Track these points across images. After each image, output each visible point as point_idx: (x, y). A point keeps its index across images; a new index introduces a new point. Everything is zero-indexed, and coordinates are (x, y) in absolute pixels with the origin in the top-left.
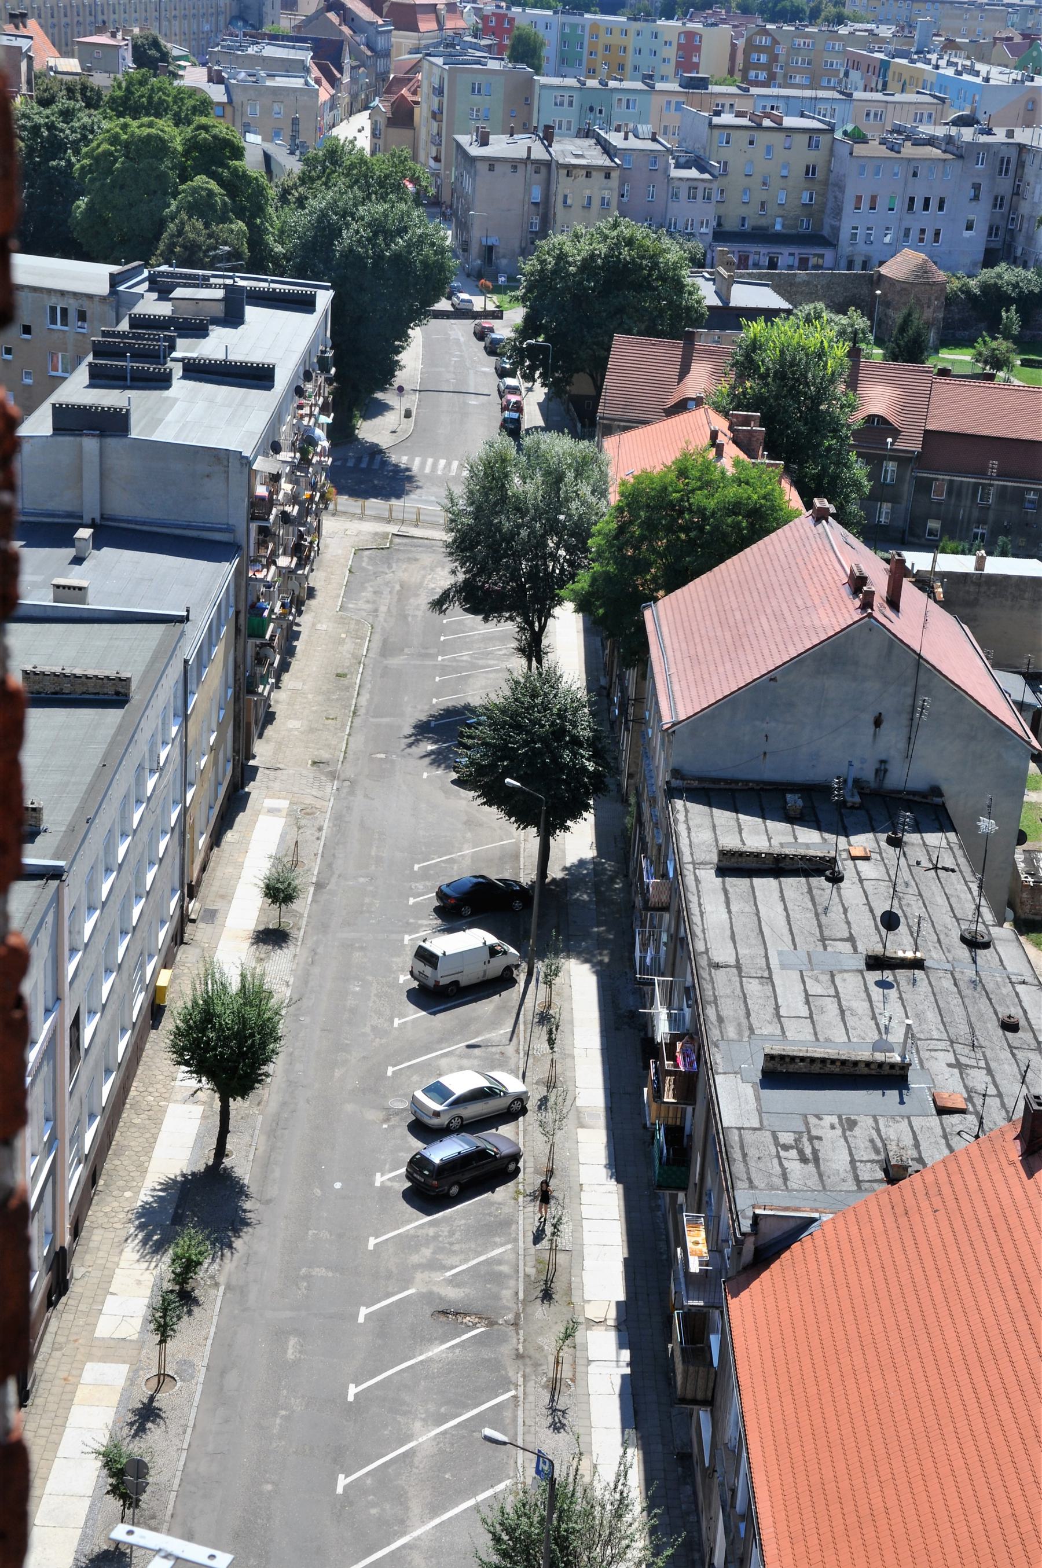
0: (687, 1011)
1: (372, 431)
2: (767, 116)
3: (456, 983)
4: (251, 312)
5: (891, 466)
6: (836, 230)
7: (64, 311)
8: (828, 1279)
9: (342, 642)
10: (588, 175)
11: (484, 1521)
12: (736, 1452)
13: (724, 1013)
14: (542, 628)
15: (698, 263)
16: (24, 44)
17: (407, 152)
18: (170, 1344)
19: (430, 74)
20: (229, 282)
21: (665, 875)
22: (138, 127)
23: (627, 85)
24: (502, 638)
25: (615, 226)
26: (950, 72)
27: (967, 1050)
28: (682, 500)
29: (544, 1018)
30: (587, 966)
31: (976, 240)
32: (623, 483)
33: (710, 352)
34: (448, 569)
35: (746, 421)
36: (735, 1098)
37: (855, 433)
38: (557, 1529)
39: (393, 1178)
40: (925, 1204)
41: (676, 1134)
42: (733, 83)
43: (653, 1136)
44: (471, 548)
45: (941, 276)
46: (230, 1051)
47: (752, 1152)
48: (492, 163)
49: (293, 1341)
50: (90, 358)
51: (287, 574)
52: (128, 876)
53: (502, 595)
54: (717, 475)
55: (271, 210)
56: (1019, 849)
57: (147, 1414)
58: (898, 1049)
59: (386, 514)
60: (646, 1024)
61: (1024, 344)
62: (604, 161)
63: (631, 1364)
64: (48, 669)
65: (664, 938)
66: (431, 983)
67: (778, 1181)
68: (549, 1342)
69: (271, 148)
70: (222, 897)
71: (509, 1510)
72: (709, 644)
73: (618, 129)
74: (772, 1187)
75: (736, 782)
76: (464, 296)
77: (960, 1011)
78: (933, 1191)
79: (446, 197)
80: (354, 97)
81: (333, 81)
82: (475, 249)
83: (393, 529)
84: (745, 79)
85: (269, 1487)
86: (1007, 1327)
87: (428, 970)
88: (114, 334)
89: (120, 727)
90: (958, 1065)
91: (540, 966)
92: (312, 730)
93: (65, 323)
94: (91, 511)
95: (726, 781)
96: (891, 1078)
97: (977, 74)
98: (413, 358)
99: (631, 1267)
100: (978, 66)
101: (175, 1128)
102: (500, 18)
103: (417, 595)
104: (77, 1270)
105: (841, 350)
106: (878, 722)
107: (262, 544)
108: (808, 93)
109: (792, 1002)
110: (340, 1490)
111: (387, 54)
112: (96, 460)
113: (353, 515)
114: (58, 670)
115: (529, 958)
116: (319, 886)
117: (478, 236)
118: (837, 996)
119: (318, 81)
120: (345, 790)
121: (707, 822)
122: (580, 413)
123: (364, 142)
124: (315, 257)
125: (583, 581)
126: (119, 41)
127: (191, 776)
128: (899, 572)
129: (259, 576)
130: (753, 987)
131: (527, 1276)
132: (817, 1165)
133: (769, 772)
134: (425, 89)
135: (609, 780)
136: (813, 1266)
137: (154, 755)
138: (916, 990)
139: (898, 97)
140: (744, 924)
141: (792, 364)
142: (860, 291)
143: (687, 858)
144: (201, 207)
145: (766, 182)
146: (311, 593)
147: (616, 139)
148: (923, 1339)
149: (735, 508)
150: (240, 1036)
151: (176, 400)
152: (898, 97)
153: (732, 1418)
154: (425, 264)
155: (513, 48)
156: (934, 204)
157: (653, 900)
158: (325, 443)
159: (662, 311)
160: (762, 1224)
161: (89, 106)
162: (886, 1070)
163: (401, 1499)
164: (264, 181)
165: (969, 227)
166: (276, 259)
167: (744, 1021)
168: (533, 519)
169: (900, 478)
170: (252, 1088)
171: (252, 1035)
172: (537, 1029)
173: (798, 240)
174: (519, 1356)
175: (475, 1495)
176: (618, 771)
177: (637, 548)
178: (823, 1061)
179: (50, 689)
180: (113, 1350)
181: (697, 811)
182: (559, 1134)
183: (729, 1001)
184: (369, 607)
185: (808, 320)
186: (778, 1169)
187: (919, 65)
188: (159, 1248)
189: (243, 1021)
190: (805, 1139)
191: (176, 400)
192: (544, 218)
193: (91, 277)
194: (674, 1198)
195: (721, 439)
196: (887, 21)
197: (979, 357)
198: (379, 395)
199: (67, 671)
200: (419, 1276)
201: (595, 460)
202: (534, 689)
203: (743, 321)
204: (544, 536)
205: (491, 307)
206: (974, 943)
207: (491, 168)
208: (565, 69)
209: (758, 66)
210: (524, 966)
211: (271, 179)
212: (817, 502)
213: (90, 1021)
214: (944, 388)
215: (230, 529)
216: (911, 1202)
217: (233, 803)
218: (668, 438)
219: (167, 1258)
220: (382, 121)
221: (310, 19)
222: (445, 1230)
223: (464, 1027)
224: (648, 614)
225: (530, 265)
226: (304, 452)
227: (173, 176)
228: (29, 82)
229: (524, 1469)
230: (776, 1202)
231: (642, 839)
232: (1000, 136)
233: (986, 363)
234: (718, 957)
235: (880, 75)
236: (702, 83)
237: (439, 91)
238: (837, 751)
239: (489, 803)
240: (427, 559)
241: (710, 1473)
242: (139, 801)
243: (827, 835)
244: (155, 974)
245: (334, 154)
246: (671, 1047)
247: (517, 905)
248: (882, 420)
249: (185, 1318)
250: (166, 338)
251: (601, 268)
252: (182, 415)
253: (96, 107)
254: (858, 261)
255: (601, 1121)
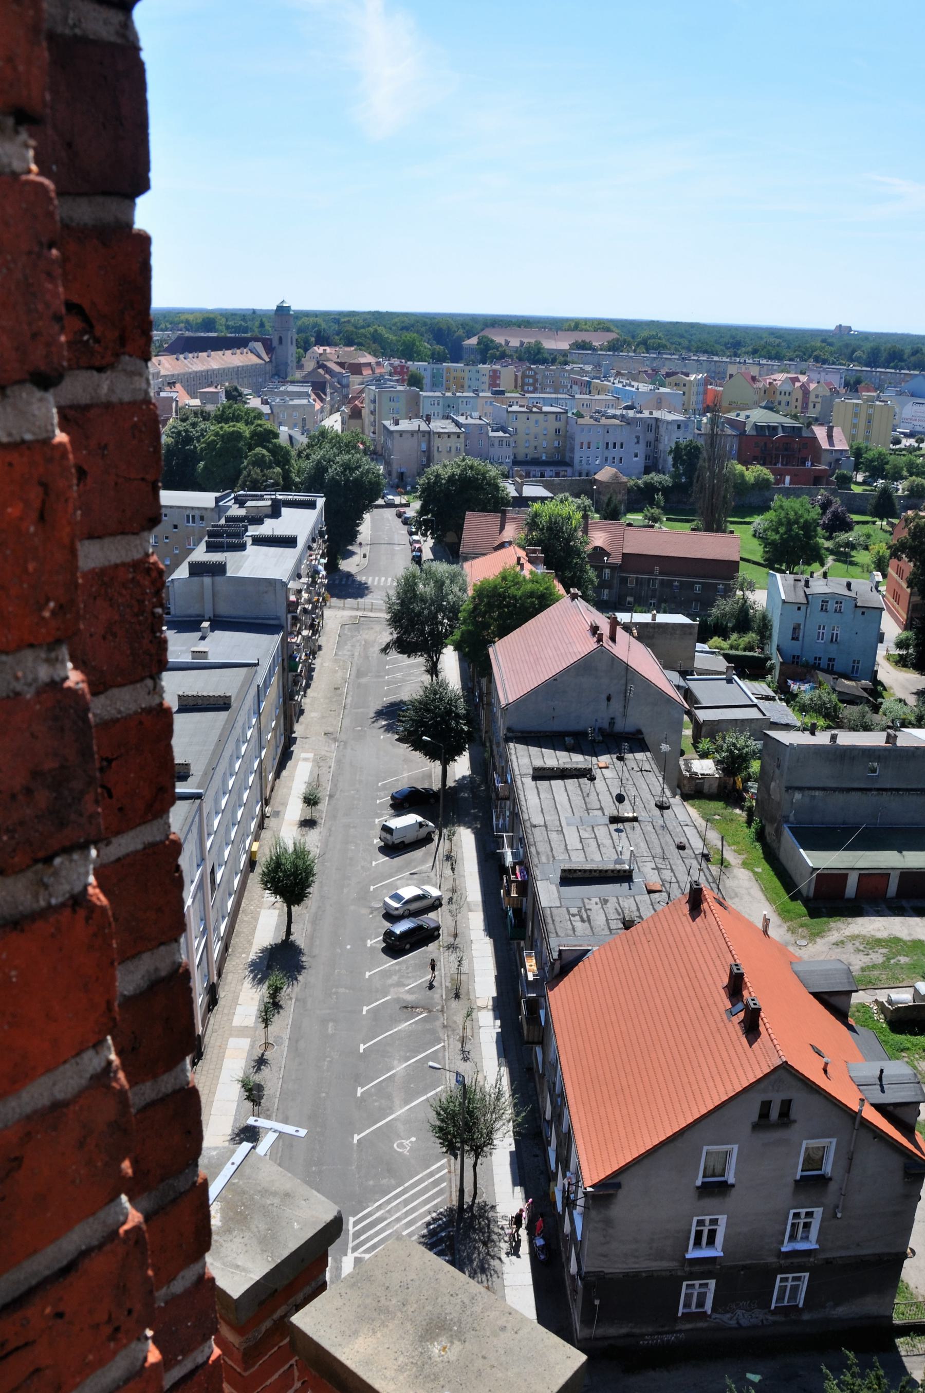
0: (521, 850)
1: (346, 565)
2: (535, 406)
3: (403, 842)
4: (284, 511)
5: (607, 571)
6: (572, 459)
7: (193, 517)
8: (597, 979)
9: (336, 672)
10: (449, 437)
11: (431, 1106)
12: (554, 1066)
13: (540, 850)
14: (438, 659)
15: (506, 476)
16: (174, 395)
17: (359, 430)
18: (270, 1028)
19: (369, 394)
20: (273, 497)
21: (506, 782)
22: (228, 428)
23: (465, 394)
24: (418, 665)
25: (464, 460)
26: (620, 386)
27: (661, 861)
28: (504, 592)
29: (449, 858)
30: (469, 830)
31: (639, 462)
32: (475, 585)
33: (515, 519)
34: (388, 632)
35: (534, 552)
36: (548, 893)
37: (589, 555)
38: (468, 1107)
39: (376, 942)
40: (643, 938)
41: (518, 912)
42: (517, 392)
43: (507, 914)
44: (399, 621)
45: (624, 479)
46: (290, 881)
47: (557, 919)
48: (401, 433)
49: (331, 1024)
50: (206, 538)
51: (307, 639)
52: (234, 796)
53: (416, 643)
54: (521, 579)
55: (293, 462)
56: (681, 759)
57: (261, 1062)
58: (627, 862)
59: (356, 606)
60: (501, 857)
61: (666, 510)
62: (457, 430)
63: (501, 1027)
64: (190, 694)
65: (508, 814)
66: (390, 843)
67: (571, 932)
68: (459, 1019)
69: (292, 433)
70: (282, 804)
71: (443, 1100)
72: (523, 664)
73: (462, 415)
74: (568, 936)
75: (540, 732)
76: (390, 497)
77: (656, 842)
78: (647, 931)
79: (379, 449)
80: (332, 406)
81: (322, 400)
82: (394, 474)
83: (360, 613)
84: (523, 390)
85: (324, 1095)
86: (685, 995)
87: (388, 836)
88: (220, 526)
89: (227, 720)
90: (657, 868)
91: (445, 831)
92: (323, 717)
93: (194, 522)
94: (209, 613)
95: (534, 732)
96: (624, 877)
97: (633, 386)
98: (367, 527)
99: (499, 980)
100: (633, 383)
101: (265, 921)
102: (402, 367)
103: (373, 646)
104: (222, 993)
105: (579, 515)
106: (609, 699)
107: (294, 625)
108: (553, 396)
109: (573, 841)
110: (359, 1095)
111: (348, 386)
112: (210, 588)
113: (339, 608)
114: (195, 694)
115: (440, 827)
116: (331, 796)
117: (396, 468)
118: (596, 838)
119: (314, 400)
120: (341, 747)
121: (526, 753)
122: (451, 551)
123: (338, 427)
124: (316, 481)
125: (457, 635)
126: (219, 389)
127: (263, 744)
128: (614, 623)
129: (293, 641)
130: (554, 836)
131: (446, 987)
132: (590, 923)
133: (557, 726)
134: (367, 401)
135: (475, 735)
136: (589, 973)
137: (245, 734)
138: (635, 833)
139: (597, 397)
140: (548, 804)
141: (555, 523)
142: (585, 487)
143: (517, 772)
144: (259, 462)
145: (536, 435)
146: (320, 648)
147: (461, 420)
148: (644, 1004)
149: (532, 594)
150: (295, 874)
151: (249, 556)
152: (597, 397)
153: (552, 1050)
154: (370, 482)
155: (409, 380)
156: (618, 445)
157: (501, 795)
158: (324, 573)
159: (489, 500)
160: (563, 954)
161: (204, 420)
162: (622, 874)
163: (389, 1097)
164: (289, 448)
165: (636, 456)
166: (296, 484)
167: (550, 853)
168: (430, 605)
169: (612, 577)
170: (303, 900)
171: (301, 874)
172: (445, 863)
173: (555, 462)
174: (444, 1027)
175: (426, 1094)
176: (480, 730)
177: (484, 617)
178: (590, 871)
179: (192, 703)
180: (242, 1032)
181: (521, 748)
182: (459, 915)
183: (542, 844)
184: (349, 653)
185: (562, 502)
186: (570, 927)
187: (605, 383)
188: (261, 982)
189: (296, 866)
190: (583, 910)
191: (249, 556)
192: (428, 458)
193: (205, 499)
194: (519, 944)
195: (522, 561)
196: (588, 364)
197: (646, 517)
198: (350, 548)
199: (200, 694)
200: (392, 990)
201: (460, 574)
202: (435, 690)
203: (530, 503)
204: (436, 614)
205: (404, 502)
206: (662, 807)
207: (401, 436)
208: (435, 389)
209: (528, 384)
210: (437, 832)
211: (292, 447)
212: (572, 590)
213: (220, 869)
214: (630, 532)
215: (278, 618)
216: (636, 938)
217: (285, 756)
218: (496, 559)
219: (265, 986)
220: (346, 417)
221: (310, 373)
222: (404, 966)
223: (408, 864)
224: (490, 650)
225: (422, 480)
226: (313, 578)
227: (245, 449)
228: (176, 412)
229: (450, 1081)
230: (570, 943)
231: (494, 764)
232: (646, 414)
233: (649, 520)
234: (535, 822)
235: (587, 387)
236: (502, 393)
237: (374, 402)
238: (591, 716)
239: (415, 749)
240: (378, 628)
241: (542, 1076)
242: (238, 758)
243: (586, 757)
244: (251, 845)
245: (323, 434)
246: (514, 869)
247: (432, 801)
248: (601, 549)
249: (276, 1015)
250: (243, 526)
251: (458, 480)
252: (253, 563)
253: (208, 420)
254: (584, 473)
255: (480, 908)
